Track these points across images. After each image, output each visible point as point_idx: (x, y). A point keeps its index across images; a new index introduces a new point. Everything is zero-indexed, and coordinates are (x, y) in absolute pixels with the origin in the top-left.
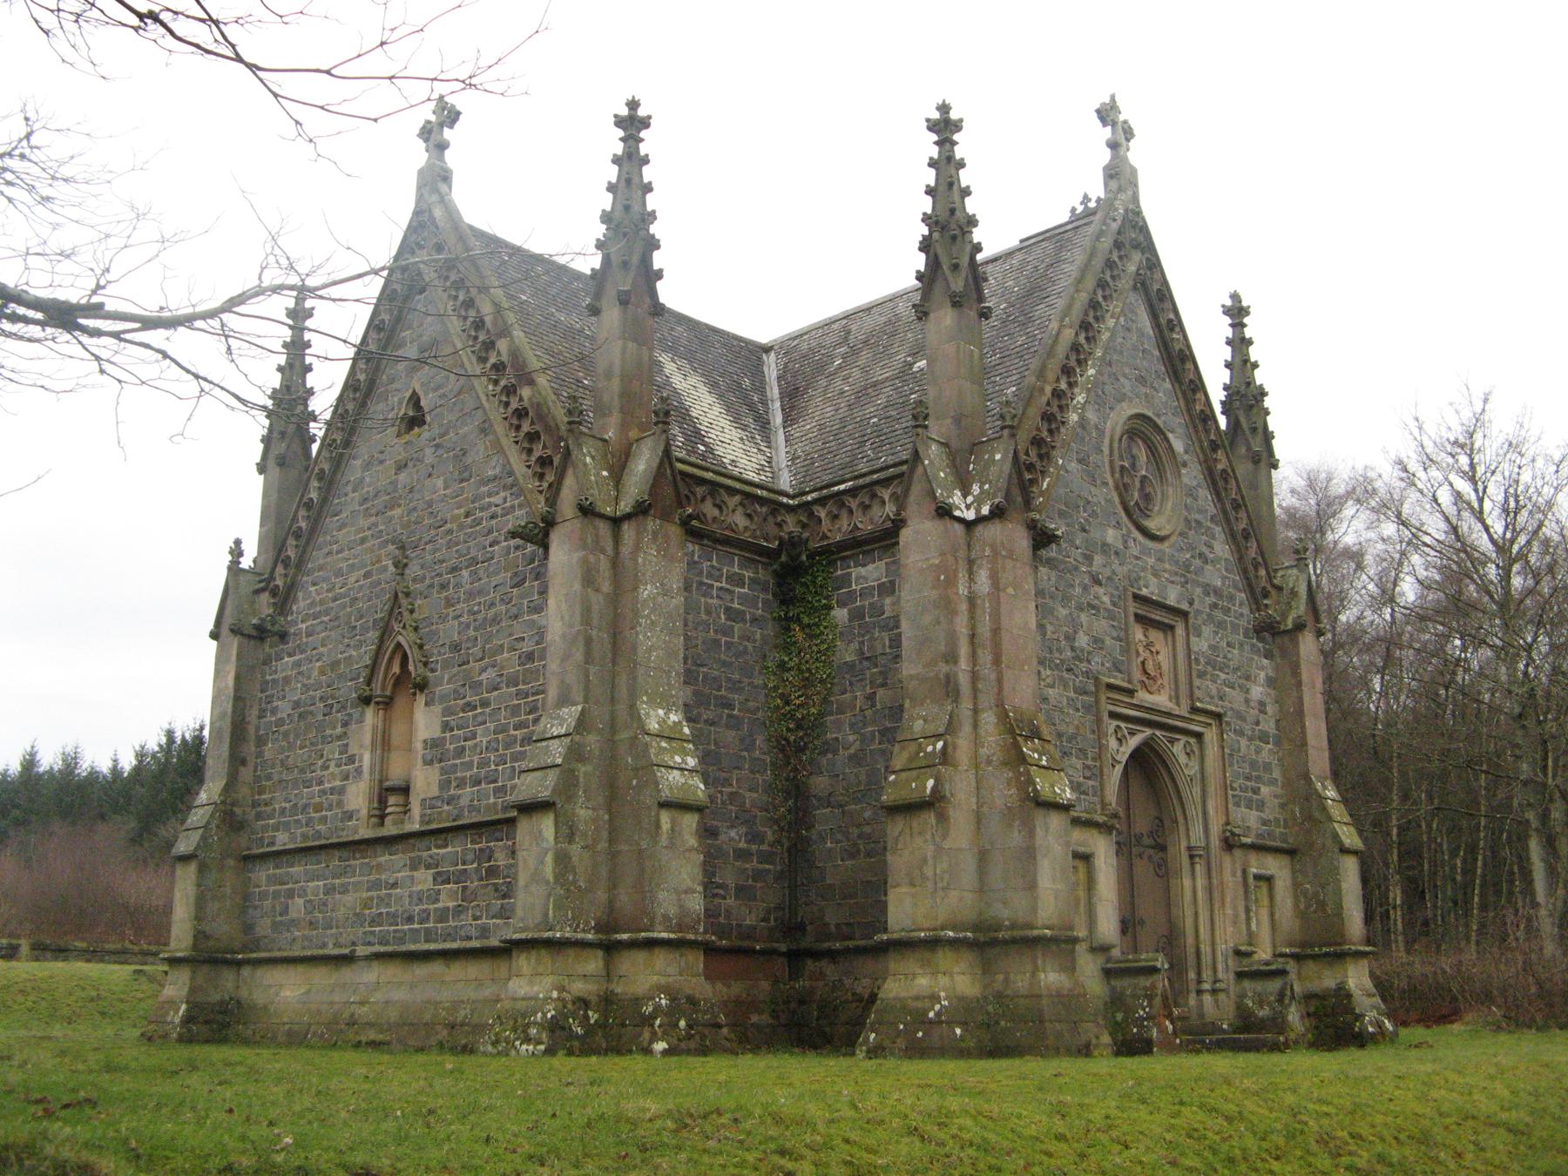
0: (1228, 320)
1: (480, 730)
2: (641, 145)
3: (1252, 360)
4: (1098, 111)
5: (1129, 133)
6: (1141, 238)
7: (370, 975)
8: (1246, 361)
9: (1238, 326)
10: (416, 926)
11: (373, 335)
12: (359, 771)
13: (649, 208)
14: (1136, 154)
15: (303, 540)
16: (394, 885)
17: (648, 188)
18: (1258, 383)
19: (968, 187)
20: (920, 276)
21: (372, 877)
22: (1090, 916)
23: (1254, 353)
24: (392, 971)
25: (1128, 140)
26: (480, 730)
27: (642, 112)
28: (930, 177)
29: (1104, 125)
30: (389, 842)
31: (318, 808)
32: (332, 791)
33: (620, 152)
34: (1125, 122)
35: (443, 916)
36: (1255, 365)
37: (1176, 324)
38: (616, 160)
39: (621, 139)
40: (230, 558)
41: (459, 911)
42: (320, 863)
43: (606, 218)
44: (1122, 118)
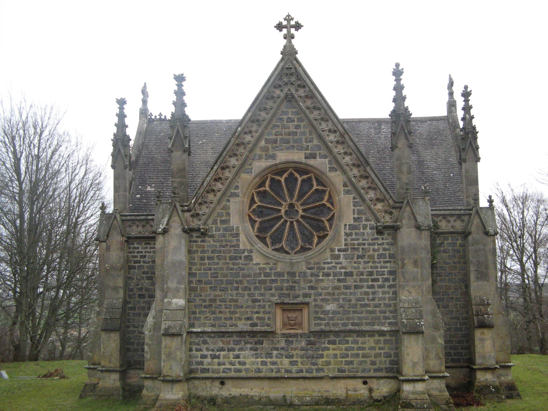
9: (398, 80)
36: (127, 126)
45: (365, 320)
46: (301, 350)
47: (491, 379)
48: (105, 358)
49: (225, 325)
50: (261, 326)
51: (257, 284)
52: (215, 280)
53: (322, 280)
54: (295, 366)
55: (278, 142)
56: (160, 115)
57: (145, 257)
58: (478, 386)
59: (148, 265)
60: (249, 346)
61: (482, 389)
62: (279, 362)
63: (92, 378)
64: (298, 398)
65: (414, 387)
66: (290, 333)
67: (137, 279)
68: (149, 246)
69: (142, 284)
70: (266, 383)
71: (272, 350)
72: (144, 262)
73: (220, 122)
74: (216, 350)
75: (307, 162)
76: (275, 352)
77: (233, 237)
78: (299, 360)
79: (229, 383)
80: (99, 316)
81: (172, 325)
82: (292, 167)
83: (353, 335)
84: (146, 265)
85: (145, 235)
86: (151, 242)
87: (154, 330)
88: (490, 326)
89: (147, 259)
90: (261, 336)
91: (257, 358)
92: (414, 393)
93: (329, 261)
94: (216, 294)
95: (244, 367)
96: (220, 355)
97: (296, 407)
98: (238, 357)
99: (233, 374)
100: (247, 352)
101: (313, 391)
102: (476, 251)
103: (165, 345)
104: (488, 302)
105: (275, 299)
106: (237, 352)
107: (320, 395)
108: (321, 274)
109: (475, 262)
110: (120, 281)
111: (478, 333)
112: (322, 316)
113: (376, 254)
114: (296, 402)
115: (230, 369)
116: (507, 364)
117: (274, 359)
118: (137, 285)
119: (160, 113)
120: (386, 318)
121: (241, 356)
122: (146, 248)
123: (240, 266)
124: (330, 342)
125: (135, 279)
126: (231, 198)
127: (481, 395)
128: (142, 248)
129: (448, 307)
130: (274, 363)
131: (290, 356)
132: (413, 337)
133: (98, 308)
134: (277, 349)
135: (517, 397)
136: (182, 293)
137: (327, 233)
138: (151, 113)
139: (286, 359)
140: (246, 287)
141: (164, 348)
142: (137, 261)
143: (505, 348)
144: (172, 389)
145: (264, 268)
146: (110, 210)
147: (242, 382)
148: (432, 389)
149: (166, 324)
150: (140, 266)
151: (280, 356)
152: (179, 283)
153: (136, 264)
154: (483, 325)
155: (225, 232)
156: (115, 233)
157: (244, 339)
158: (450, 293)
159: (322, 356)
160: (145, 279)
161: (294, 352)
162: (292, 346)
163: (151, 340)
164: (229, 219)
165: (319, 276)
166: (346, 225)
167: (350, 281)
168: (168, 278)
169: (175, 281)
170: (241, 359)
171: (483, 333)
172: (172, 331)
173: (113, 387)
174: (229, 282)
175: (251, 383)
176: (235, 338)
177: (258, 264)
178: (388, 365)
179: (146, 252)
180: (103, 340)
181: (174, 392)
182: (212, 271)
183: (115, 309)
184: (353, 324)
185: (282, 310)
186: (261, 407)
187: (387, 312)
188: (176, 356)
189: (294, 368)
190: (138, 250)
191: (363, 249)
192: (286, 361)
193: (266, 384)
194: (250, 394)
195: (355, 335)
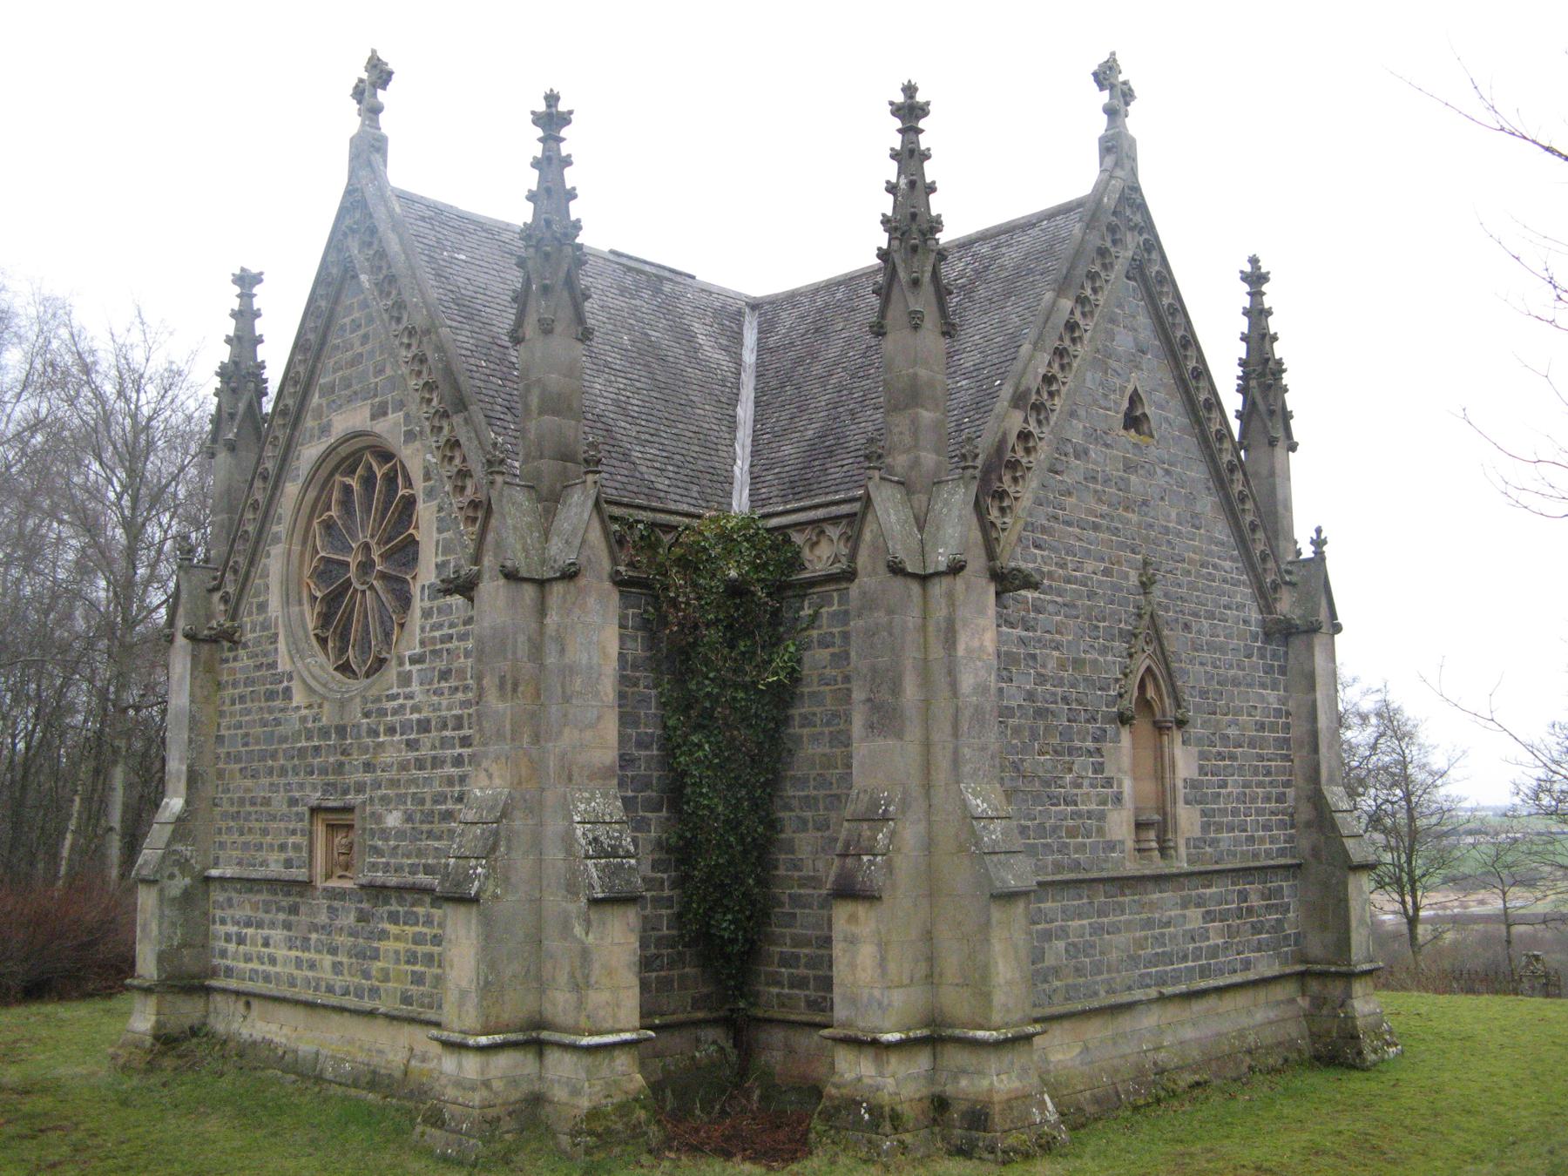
0: (1247, 288)
2: (562, 145)
3: (1272, 332)
4: (1095, 75)
5: (1127, 95)
7: (1149, 1020)
8: (1263, 336)
9: (1256, 295)
10: (1190, 964)
11: (1138, 201)
12: (1118, 799)
14: (1136, 122)
15: (271, 482)
16: (1168, 924)
20: (883, 255)
21: (1144, 916)
22: (928, 763)
23: (1274, 325)
24: (1172, 1012)
25: (1127, 104)
27: (562, 107)
28: (891, 170)
29: (1101, 90)
30: (1159, 880)
31: (1072, 833)
32: (1090, 815)
34: (1125, 83)
35: (1214, 952)
36: (1274, 338)
38: (536, 164)
39: (540, 140)
41: (1227, 945)
42: (1081, 898)
44: (1121, 78)
46: (351, 935)
47: (871, 1077)
58: (831, 1098)
61: (838, 1109)
65: (460, 1065)
71: (310, 932)
76: (314, 936)
88: (869, 897)
92: (459, 1084)
93: (395, 690)
102: (871, 633)
104: (885, 811)
105: (315, 797)
109: (865, 670)
111: (841, 913)
114: (329, 1074)
116: (971, 1033)
124: (394, 918)
127: (831, 1127)
129: (828, 828)
130: (312, 966)
132: (462, 910)
135: (986, 1155)
143: (977, 976)
147: (270, 1006)
148: (559, 1081)
154: (848, 891)
158: (834, 781)
171: (853, 918)
185: (328, 825)
192: (328, 960)
193: (299, 1016)
194: (277, 1039)
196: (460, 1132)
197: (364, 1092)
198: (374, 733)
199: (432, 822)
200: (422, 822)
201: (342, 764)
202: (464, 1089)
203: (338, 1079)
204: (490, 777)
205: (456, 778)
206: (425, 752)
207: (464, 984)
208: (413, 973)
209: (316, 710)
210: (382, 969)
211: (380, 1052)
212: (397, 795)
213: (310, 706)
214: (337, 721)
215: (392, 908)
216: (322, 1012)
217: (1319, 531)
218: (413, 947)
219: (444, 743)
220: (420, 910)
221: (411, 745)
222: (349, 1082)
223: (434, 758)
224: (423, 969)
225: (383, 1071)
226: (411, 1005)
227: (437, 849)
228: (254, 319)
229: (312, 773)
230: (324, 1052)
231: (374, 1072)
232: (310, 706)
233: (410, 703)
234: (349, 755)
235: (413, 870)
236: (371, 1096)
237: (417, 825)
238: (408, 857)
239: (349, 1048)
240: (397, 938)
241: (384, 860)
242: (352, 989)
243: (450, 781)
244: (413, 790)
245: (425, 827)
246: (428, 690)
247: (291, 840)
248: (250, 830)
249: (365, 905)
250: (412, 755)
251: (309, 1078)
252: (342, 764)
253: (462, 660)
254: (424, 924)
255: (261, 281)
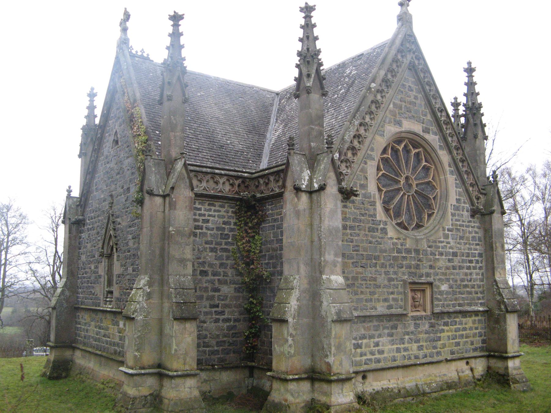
0: (466, 74)
1: (227, 310)
3: (477, 92)
6: (413, 47)
9: (470, 76)
13: (318, 48)
17: (316, 38)
18: (479, 102)
19: (317, 36)
23: (477, 89)
26: (227, 310)
33: (303, 24)
37: (432, 83)
39: (304, 18)
40: (67, 193)
43: (299, 54)
45: (466, 300)
46: (426, 333)
48: (179, 358)
49: (365, 308)
50: (395, 309)
51: (392, 262)
52: (356, 254)
53: (438, 259)
54: (422, 351)
55: (403, 109)
56: (142, 51)
57: (208, 221)
59: (212, 232)
60: (386, 331)
62: (409, 348)
63: (140, 388)
64: (427, 386)
66: (417, 316)
67: (199, 250)
68: (213, 208)
69: (205, 258)
70: (400, 372)
71: (404, 335)
72: (207, 229)
73: (207, 78)
74: (358, 338)
75: (424, 136)
76: (407, 337)
77: (371, 205)
78: (424, 344)
79: (370, 376)
80: (149, 299)
81: (341, 308)
82: (408, 138)
83: (459, 315)
84: (209, 232)
85: (211, 193)
86: (216, 203)
87: (298, 316)
89: (210, 225)
90: (396, 320)
91: (393, 344)
93: (442, 240)
94: (357, 271)
95: (382, 356)
96: (362, 343)
97: (429, 395)
98: (377, 345)
99: (373, 366)
100: (384, 338)
101: (436, 376)
103: (335, 334)
106: (376, 340)
107: (441, 379)
108: (437, 253)
110: (189, 251)
112: (439, 296)
113: (471, 235)
114: (427, 390)
115: (370, 360)
117: (406, 345)
118: (198, 258)
119: (143, 50)
120: (479, 299)
121: (380, 344)
122: (210, 210)
123: (378, 239)
124: (446, 324)
125: (196, 250)
126: (368, 160)
128: (205, 210)
130: (406, 350)
131: (418, 340)
133: (149, 288)
134: (408, 334)
136: (339, 269)
137: (434, 211)
138: (131, 47)
139: (415, 344)
140: (383, 264)
141: (334, 338)
142: (198, 226)
144: (342, 390)
145: (396, 243)
146: (76, 193)
147: (381, 373)
149: (334, 307)
150: (202, 233)
151: (411, 341)
152: (336, 255)
153: (197, 231)
155: (364, 199)
156: (182, 185)
157: (382, 323)
159: (439, 339)
160: (208, 250)
161: (421, 336)
162: (419, 329)
163: (295, 329)
164: (367, 184)
165: (435, 255)
166: (451, 205)
167: (456, 261)
168: (325, 249)
169: (332, 253)
170: (380, 348)
172: (345, 316)
173: (190, 398)
174: (369, 258)
175: (389, 374)
176: (376, 323)
177: (392, 238)
178: (481, 345)
179: (209, 216)
180: (175, 332)
181: (345, 394)
182: (354, 244)
183: (186, 289)
184: (460, 305)
186: (402, 399)
187: (479, 293)
188: (346, 348)
189: (421, 353)
190: (200, 212)
191: (463, 230)
192: (415, 346)
193: (400, 373)
194: (391, 386)
195: (460, 316)
196: (524, 382)
197: (447, 391)
198: (433, 254)
199: (460, 289)
200: (456, 288)
201: (418, 265)
202: (517, 369)
203: (434, 391)
204: (500, 274)
205: (469, 274)
206: (456, 263)
207: (514, 338)
208: (456, 342)
209: (402, 241)
210: (442, 344)
211: (444, 375)
212: (445, 278)
213: (399, 239)
214: (414, 247)
215: (445, 320)
216: (413, 368)
217: (70, 187)
218: (455, 333)
219: (463, 261)
220: (457, 320)
221: (449, 261)
222: (439, 389)
223: (460, 266)
224: (460, 340)
225: (450, 381)
226: (455, 354)
227: (463, 298)
228: (313, 28)
229: (402, 267)
230: (420, 383)
231: (447, 383)
232: (399, 239)
233: (449, 245)
234: (422, 261)
235: (454, 306)
236: (450, 391)
237: (454, 289)
238: (451, 301)
239: (431, 378)
240: (447, 331)
241: (441, 303)
242: (428, 355)
243: (466, 274)
244: (452, 277)
245: (458, 290)
246: (456, 242)
247: (391, 296)
248: (362, 292)
249: (433, 321)
250: (450, 264)
251: (419, 395)
252: (418, 265)
253: (468, 234)
254: (459, 324)
255: (314, 9)
